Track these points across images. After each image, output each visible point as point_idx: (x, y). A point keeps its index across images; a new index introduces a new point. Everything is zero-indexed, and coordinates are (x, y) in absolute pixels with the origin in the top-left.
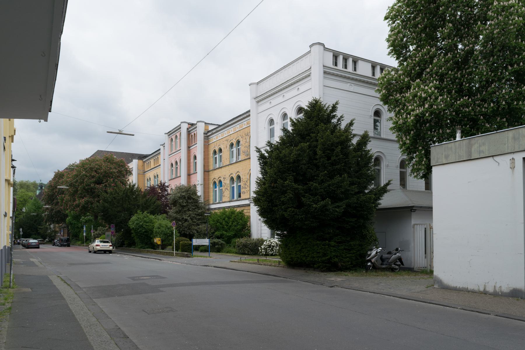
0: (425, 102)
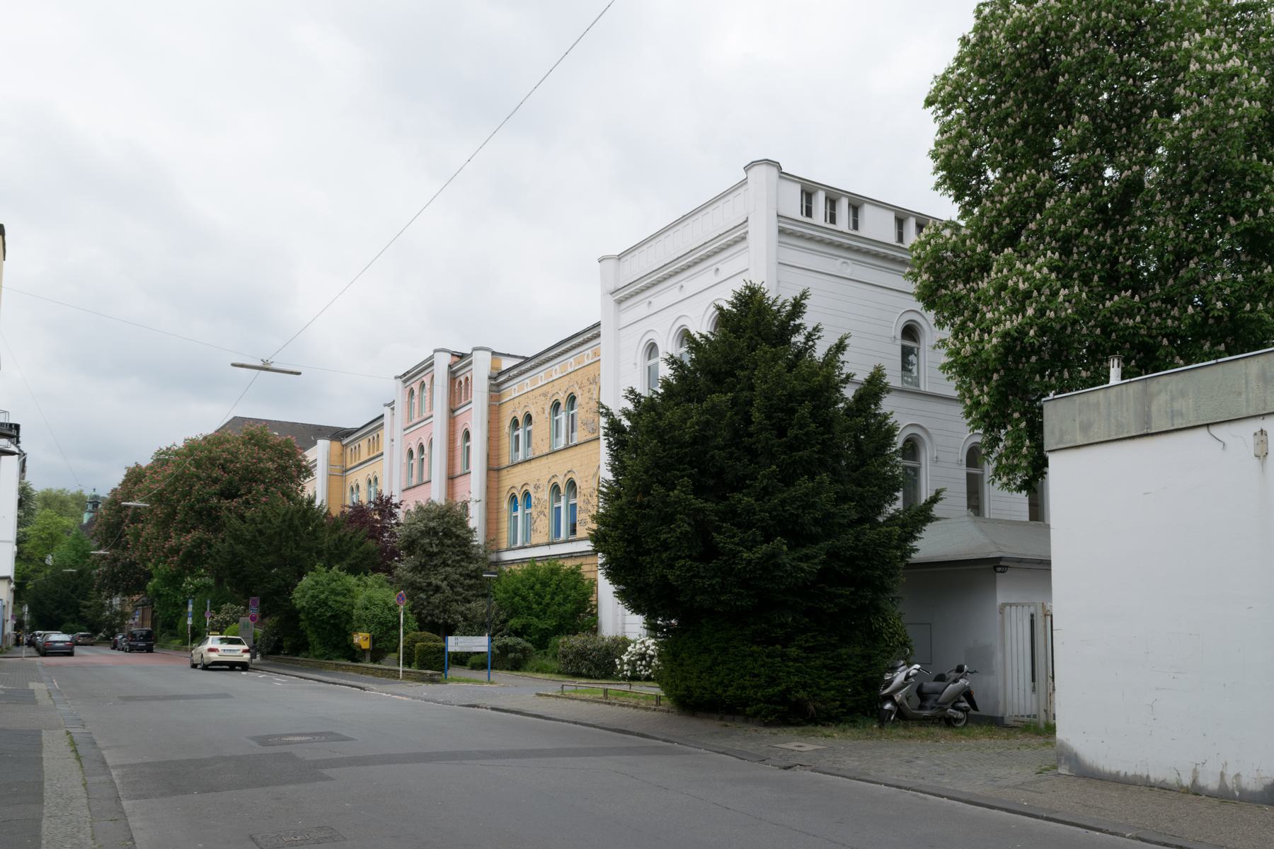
0: (1027, 302)
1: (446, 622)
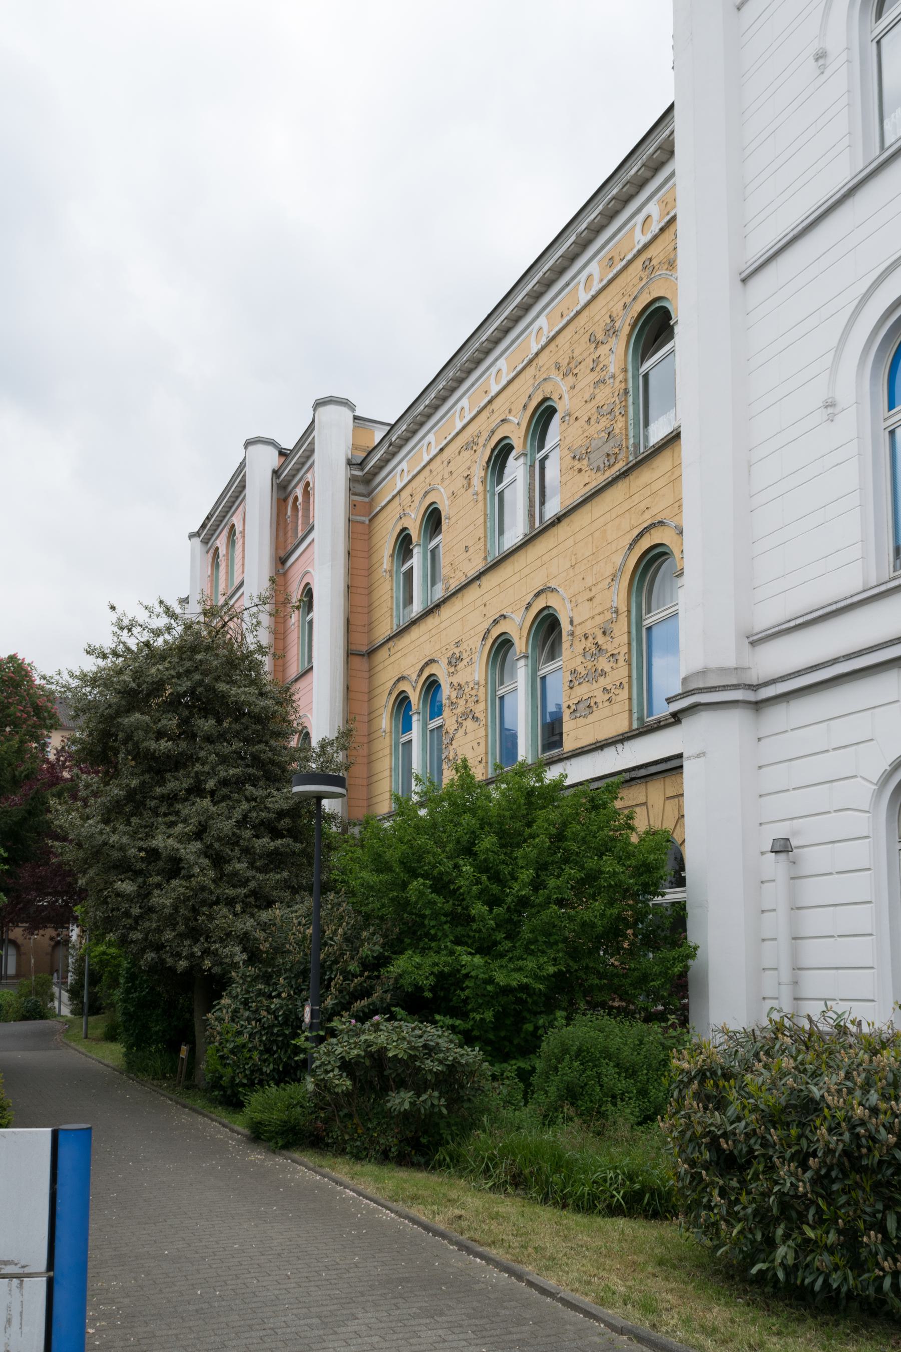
1: (194, 968)
